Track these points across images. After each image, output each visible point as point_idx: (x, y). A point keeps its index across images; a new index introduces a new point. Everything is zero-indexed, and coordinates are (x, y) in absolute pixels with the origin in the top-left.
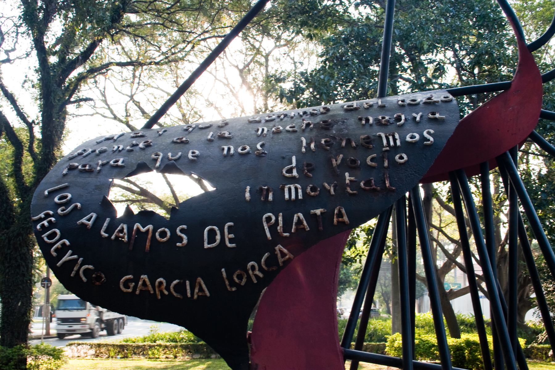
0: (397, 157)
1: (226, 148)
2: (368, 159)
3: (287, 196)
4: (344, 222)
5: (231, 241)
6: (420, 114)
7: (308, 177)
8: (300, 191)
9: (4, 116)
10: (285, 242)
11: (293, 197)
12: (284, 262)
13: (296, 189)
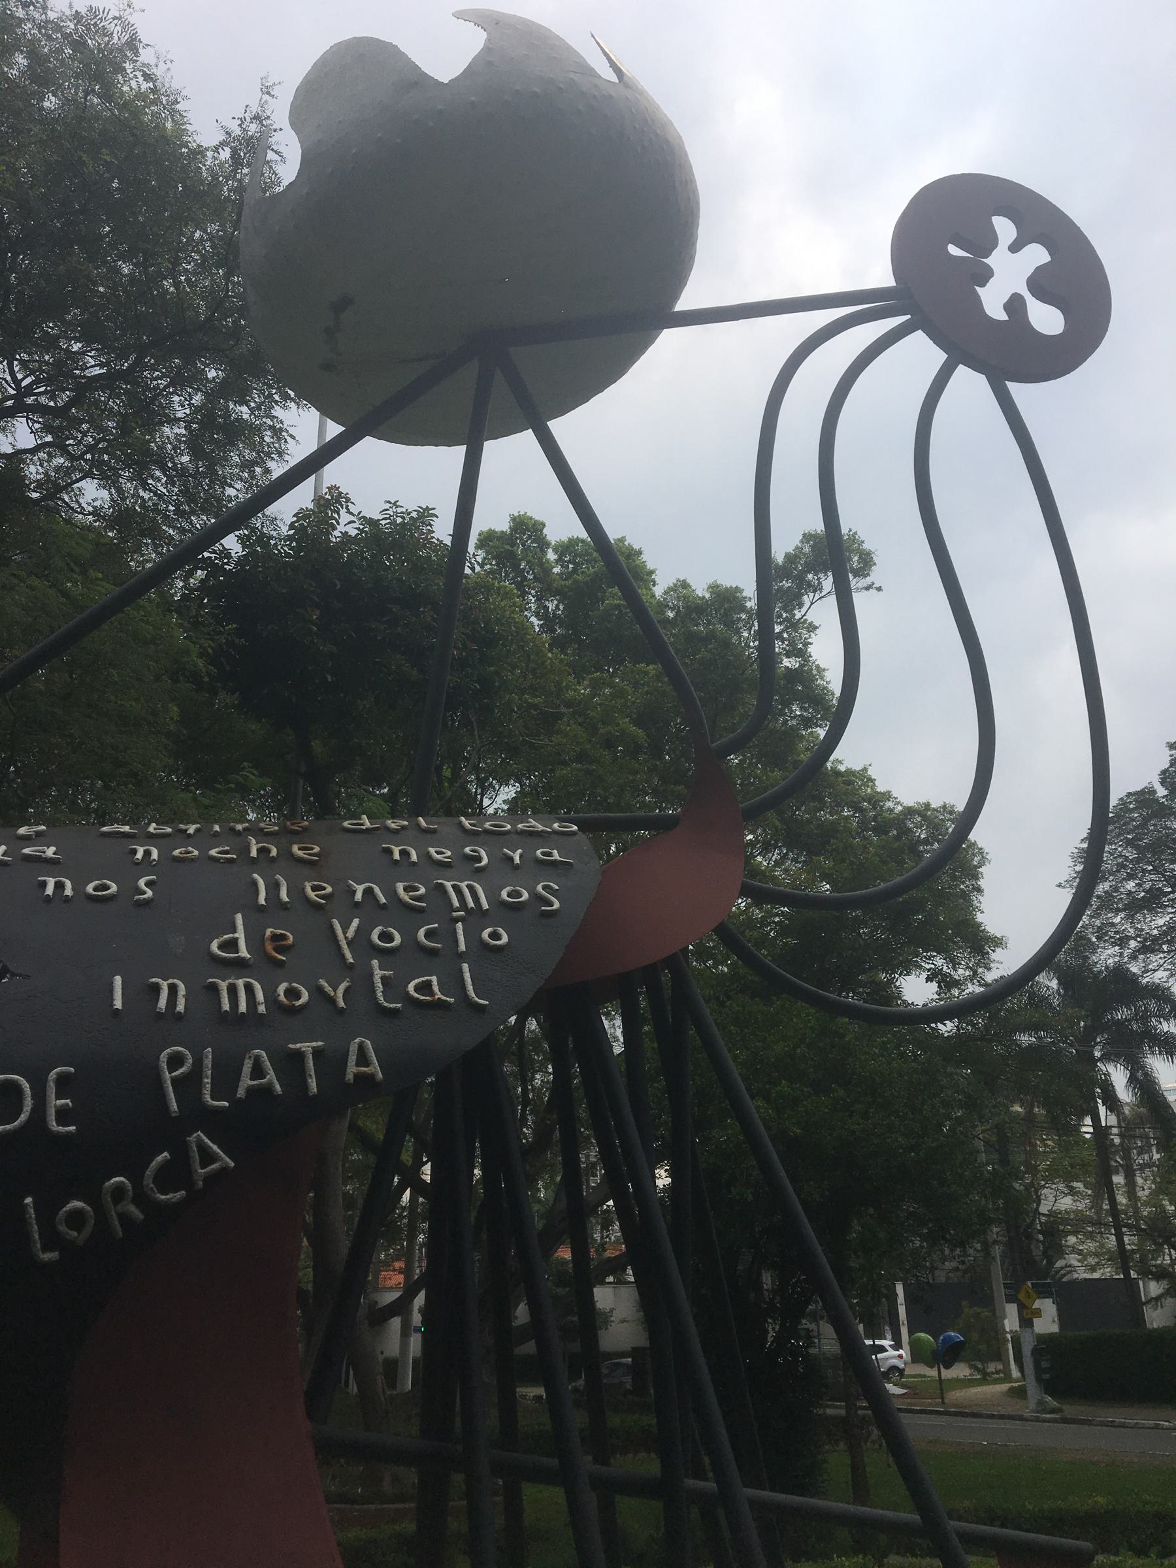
0: (485, 934)
1: (51, 883)
2: (421, 933)
3: (226, 1006)
4: (371, 1077)
5: (63, 1116)
6: (520, 851)
7: (281, 964)
8: (260, 996)
9: (404, 53)
10: (211, 1121)
11: (243, 1007)
12: (207, 1179)
13: (249, 988)
